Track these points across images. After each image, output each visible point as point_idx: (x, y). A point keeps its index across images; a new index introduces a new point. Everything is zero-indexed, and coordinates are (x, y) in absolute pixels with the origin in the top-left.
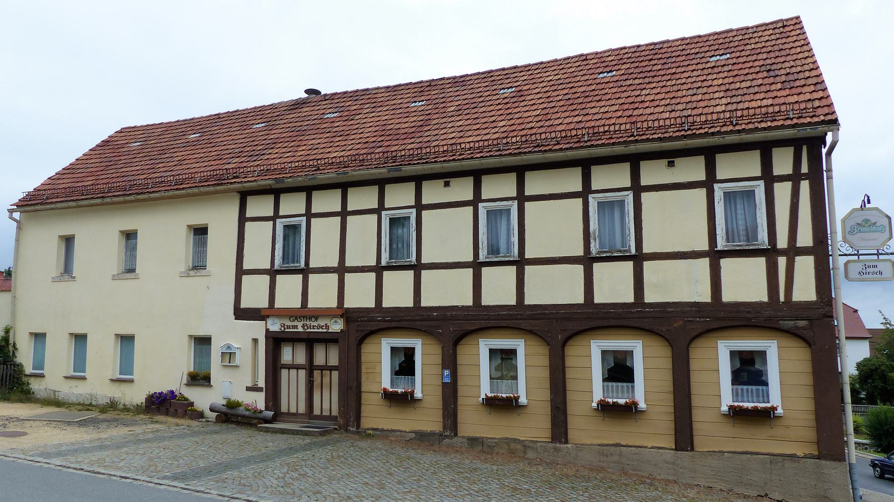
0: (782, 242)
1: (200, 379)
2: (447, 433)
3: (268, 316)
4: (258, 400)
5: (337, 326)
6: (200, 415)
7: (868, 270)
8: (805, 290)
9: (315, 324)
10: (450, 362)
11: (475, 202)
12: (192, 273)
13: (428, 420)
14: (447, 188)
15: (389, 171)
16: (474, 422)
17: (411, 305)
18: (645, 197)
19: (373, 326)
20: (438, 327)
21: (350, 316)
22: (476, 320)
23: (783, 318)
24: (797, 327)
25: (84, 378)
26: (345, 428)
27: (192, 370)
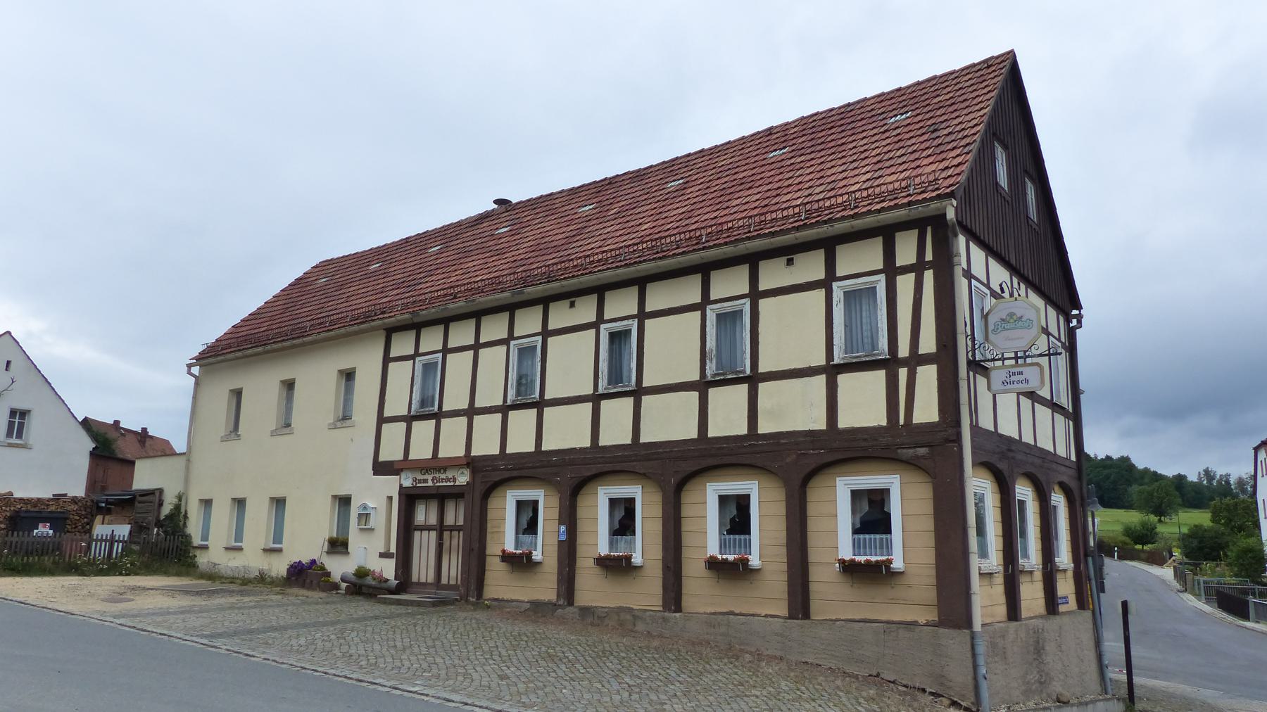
0: (904, 351)
1: (338, 545)
2: (561, 602)
3: (402, 470)
4: (388, 569)
5: (463, 478)
6: (335, 587)
7: (1013, 378)
8: (927, 410)
9: (443, 476)
10: (569, 517)
11: (826, 284)
12: (339, 424)
13: (544, 588)
14: (792, 268)
15: (513, 295)
16: (593, 589)
17: (629, 441)
18: (764, 304)
19: (497, 477)
20: (557, 474)
21: (471, 462)
22: (704, 457)
23: (902, 446)
24: (917, 457)
25: (240, 549)
26: (464, 598)
27: (335, 535)
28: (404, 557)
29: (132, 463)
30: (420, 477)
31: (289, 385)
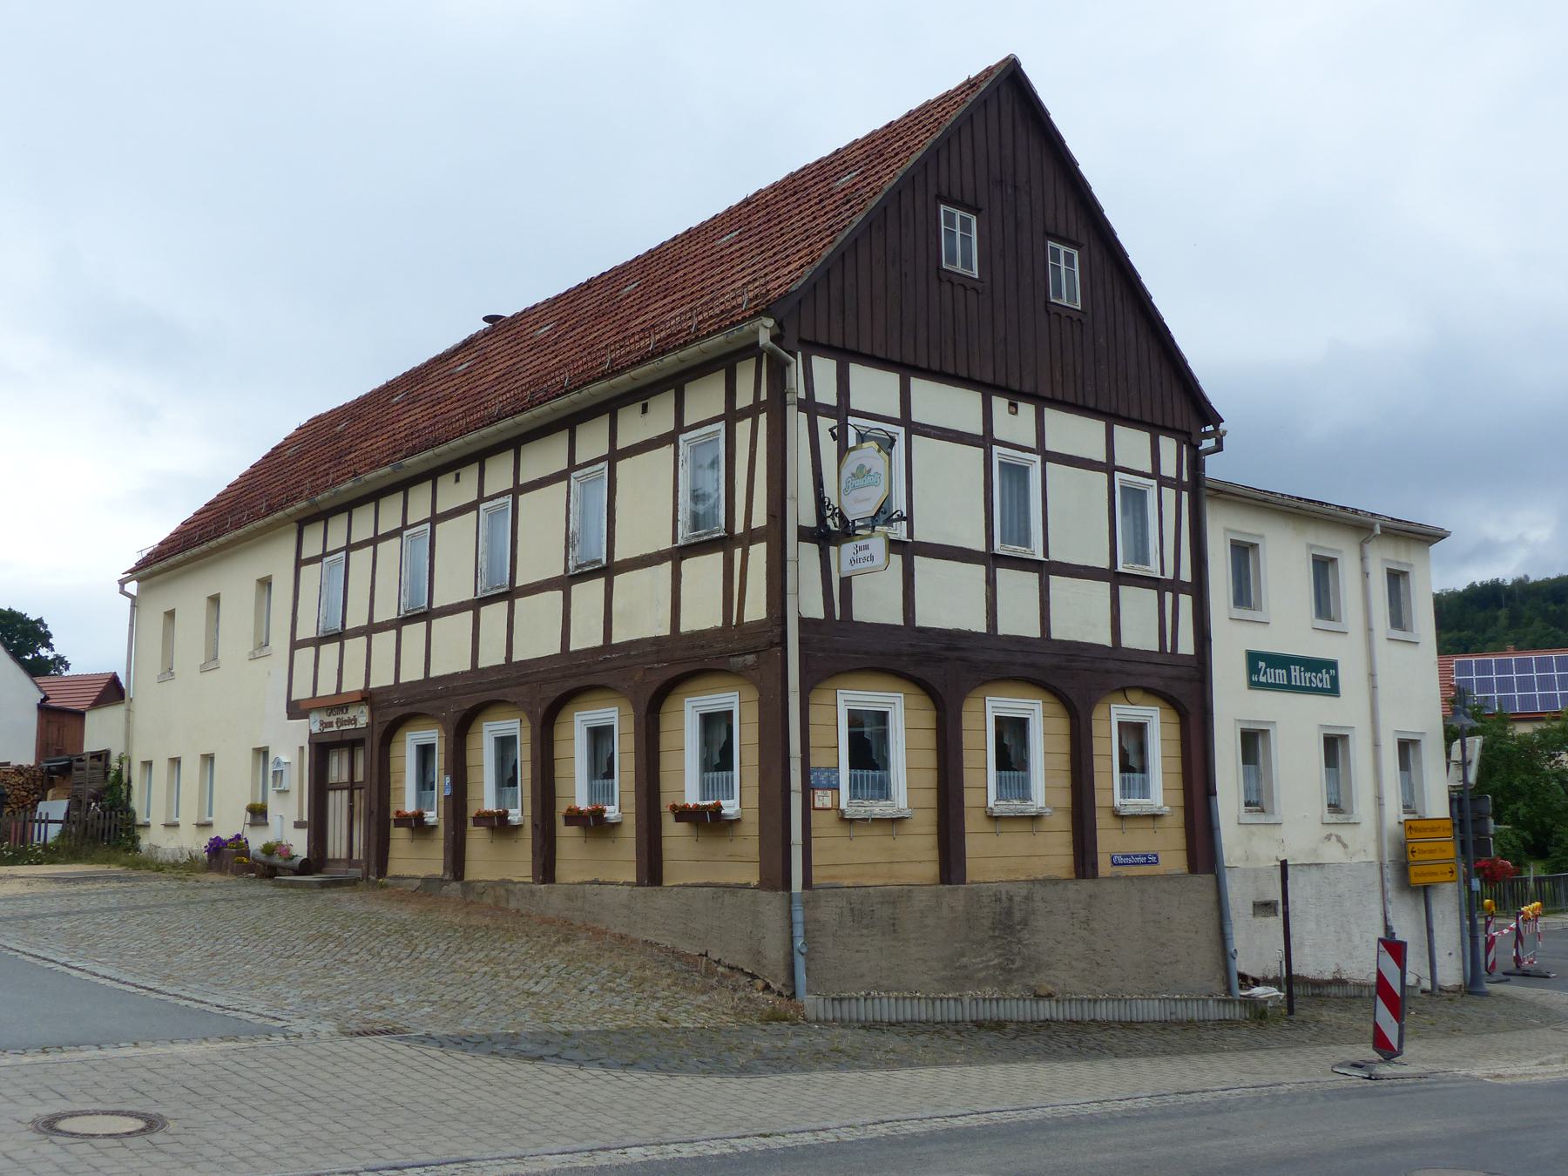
1: (258, 814)
4: (299, 844)
21: (368, 697)
25: (176, 825)
28: (317, 825)
29: (80, 715)
30: (327, 719)
31: (215, 600)
